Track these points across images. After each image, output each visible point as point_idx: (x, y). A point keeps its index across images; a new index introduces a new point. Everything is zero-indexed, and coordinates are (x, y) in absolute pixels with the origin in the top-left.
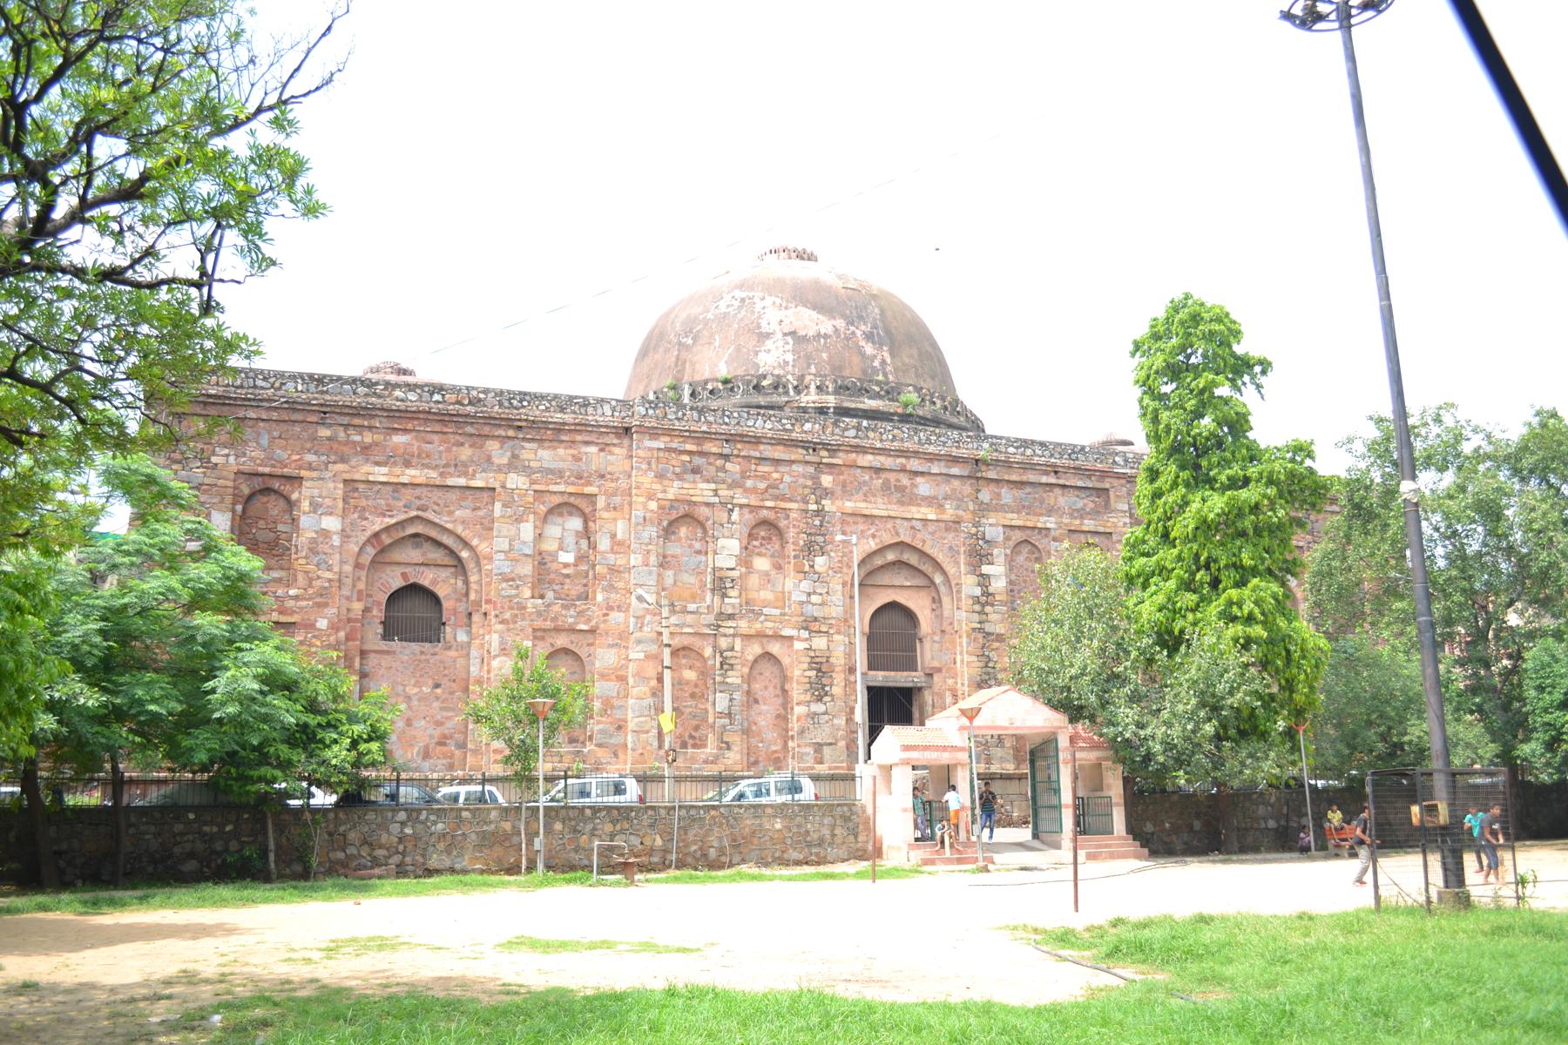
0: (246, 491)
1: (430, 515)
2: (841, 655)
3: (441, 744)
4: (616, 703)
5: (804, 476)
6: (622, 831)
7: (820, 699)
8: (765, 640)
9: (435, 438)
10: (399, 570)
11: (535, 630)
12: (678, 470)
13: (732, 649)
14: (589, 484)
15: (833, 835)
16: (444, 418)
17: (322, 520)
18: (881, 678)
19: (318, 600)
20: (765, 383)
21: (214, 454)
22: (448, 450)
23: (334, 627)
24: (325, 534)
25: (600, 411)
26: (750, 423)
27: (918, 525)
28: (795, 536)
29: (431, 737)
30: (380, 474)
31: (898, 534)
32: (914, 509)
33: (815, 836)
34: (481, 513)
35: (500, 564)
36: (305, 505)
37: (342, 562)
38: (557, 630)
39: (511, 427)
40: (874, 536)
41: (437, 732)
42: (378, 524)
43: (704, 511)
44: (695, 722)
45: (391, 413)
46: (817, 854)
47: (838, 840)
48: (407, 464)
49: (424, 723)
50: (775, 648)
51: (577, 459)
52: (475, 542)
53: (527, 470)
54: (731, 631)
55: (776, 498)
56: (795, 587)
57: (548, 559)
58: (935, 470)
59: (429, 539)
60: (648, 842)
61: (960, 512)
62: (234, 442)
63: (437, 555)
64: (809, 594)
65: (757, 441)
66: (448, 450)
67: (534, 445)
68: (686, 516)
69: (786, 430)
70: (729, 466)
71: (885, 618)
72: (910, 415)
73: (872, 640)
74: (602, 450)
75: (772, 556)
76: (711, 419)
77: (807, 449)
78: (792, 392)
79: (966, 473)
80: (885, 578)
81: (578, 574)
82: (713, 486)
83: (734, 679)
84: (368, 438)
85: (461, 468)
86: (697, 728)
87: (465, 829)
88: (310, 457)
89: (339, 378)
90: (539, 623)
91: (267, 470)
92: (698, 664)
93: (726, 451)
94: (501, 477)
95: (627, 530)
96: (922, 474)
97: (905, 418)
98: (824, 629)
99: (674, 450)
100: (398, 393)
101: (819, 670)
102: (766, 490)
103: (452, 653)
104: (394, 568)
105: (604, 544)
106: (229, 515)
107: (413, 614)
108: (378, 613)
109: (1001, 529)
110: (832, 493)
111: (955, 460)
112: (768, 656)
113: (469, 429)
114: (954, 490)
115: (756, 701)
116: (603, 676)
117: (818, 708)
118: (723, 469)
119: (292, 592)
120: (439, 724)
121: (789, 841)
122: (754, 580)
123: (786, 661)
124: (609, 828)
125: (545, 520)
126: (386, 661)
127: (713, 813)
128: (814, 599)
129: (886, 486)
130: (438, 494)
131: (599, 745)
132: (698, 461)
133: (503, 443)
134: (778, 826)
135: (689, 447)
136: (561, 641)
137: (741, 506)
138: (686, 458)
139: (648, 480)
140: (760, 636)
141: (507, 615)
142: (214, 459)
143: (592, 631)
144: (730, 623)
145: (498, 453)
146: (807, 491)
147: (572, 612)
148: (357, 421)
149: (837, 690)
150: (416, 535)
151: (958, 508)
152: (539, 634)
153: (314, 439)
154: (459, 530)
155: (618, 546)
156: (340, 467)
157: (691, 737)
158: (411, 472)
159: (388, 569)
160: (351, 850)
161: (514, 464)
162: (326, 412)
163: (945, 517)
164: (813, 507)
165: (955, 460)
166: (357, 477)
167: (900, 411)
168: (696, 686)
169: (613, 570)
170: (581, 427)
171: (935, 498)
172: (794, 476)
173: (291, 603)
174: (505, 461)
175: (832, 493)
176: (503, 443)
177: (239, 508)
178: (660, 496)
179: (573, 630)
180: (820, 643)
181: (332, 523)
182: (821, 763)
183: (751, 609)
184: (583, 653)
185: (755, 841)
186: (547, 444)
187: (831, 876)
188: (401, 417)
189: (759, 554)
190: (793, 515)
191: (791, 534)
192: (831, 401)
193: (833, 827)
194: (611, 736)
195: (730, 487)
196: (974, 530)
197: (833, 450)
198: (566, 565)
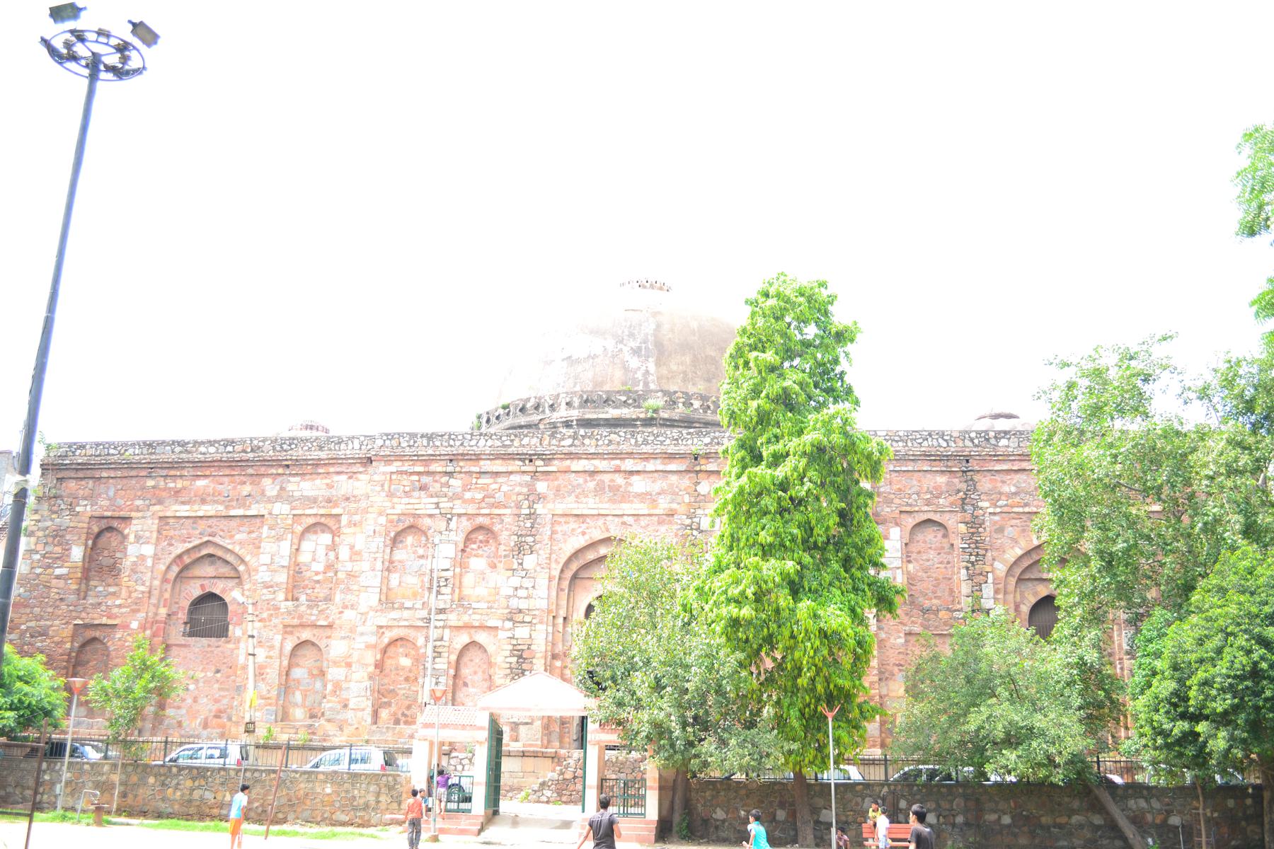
0: (96, 529)
1: (217, 540)
2: (543, 642)
3: (217, 716)
4: (344, 685)
5: (520, 485)
6: (199, 787)
8: (473, 631)
9: (226, 479)
10: (199, 582)
11: (285, 626)
12: (407, 489)
13: (441, 639)
14: (336, 506)
15: (378, 802)
16: (232, 464)
17: (142, 550)
19: (134, 607)
21: (78, 505)
22: (234, 488)
23: (143, 628)
24: (142, 558)
25: (350, 446)
26: (473, 443)
27: (630, 520)
28: (507, 539)
29: (210, 711)
30: (183, 510)
31: (608, 530)
32: (624, 506)
33: (362, 801)
34: (254, 535)
35: (263, 576)
36: (132, 538)
37: (153, 578)
38: (302, 626)
39: (281, 466)
40: (584, 533)
42: (180, 548)
43: (428, 521)
44: (408, 703)
45: (197, 464)
46: (361, 817)
47: (383, 806)
48: (203, 501)
49: (220, 702)
50: (481, 637)
51: (330, 486)
52: (247, 559)
53: (290, 499)
54: (441, 624)
55: (492, 506)
56: (503, 581)
57: (304, 568)
59: (220, 558)
60: (219, 797)
61: (674, 506)
62: (91, 497)
63: (224, 570)
64: (516, 589)
65: (477, 458)
66: (234, 488)
67: (298, 479)
68: (411, 527)
69: (504, 446)
70: (452, 482)
72: (652, 419)
74: (350, 478)
76: (438, 443)
77: (523, 460)
78: (547, 411)
79: (683, 468)
81: (326, 580)
82: (435, 500)
83: (442, 664)
84: (180, 484)
85: (242, 501)
86: (409, 707)
87: (84, 778)
88: (139, 502)
89: (164, 442)
90: (288, 621)
91: (109, 514)
92: (413, 652)
93: (450, 469)
94: (269, 506)
95: (363, 539)
96: (638, 472)
97: (648, 422)
98: (528, 619)
99: (406, 473)
100: (202, 449)
101: (520, 657)
102: (483, 500)
105: (344, 553)
106: (82, 548)
107: (208, 616)
108: (183, 616)
110: (545, 498)
111: (671, 457)
112: (473, 643)
113: (250, 471)
115: (466, 685)
116: (336, 663)
118: (447, 485)
119: (118, 602)
120: (217, 701)
121: (337, 805)
122: (468, 580)
123: (491, 649)
124: (189, 783)
125: (302, 536)
126: (183, 652)
127: (273, 776)
128: (522, 593)
130: (224, 522)
131: (329, 721)
132: (425, 479)
133: (274, 479)
134: (328, 790)
136: (306, 635)
137: (459, 515)
138: (415, 478)
139: (380, 499)
140: (467, 627)
141: (265, 615)
142: (78, 509)
143: (330, 626)
145: (270, 487)
146: (521, 497)
147: (315, 612)
148: (172, 472)
150: (211, 556)
152: (288, 629)
153: (143, 488)
154: (237, 549)
155: (355, 554)
156: (157, 508)
157: (403, 714)
159: (192, 582)
160: (10, 790)
161: (282, 496)
162: (152, 468)
163: (657, 512)
164: (527, 511)
165: (671, 457)
166: (168, 514)
167: (642, 416)
168: (410, 671)
169: (350, 575)
170: (334, 461)
171: (647, 494)
172: (514, 485)
173: (115, 610)
174: (275, 493)
175: (545, 498)
176: (274, 479)
177: (90, 542)
178: (389, 511)
179: (315, 626)
180: (522, 632)
181: (148, 550)
182: (517, 740)
183: (462, 603)
184: (322, 644)
185: (308, 802)
186: (308, 477)
187: (284, 833)
188: (203, 467)
190: (507, 520)
191: (504, 536)
192: (575, 414)
193: (378, 794)
194: (338, 713)
195: (451, 499)
196: (688, 522)
197: (547, 459)
198: (317, 573)
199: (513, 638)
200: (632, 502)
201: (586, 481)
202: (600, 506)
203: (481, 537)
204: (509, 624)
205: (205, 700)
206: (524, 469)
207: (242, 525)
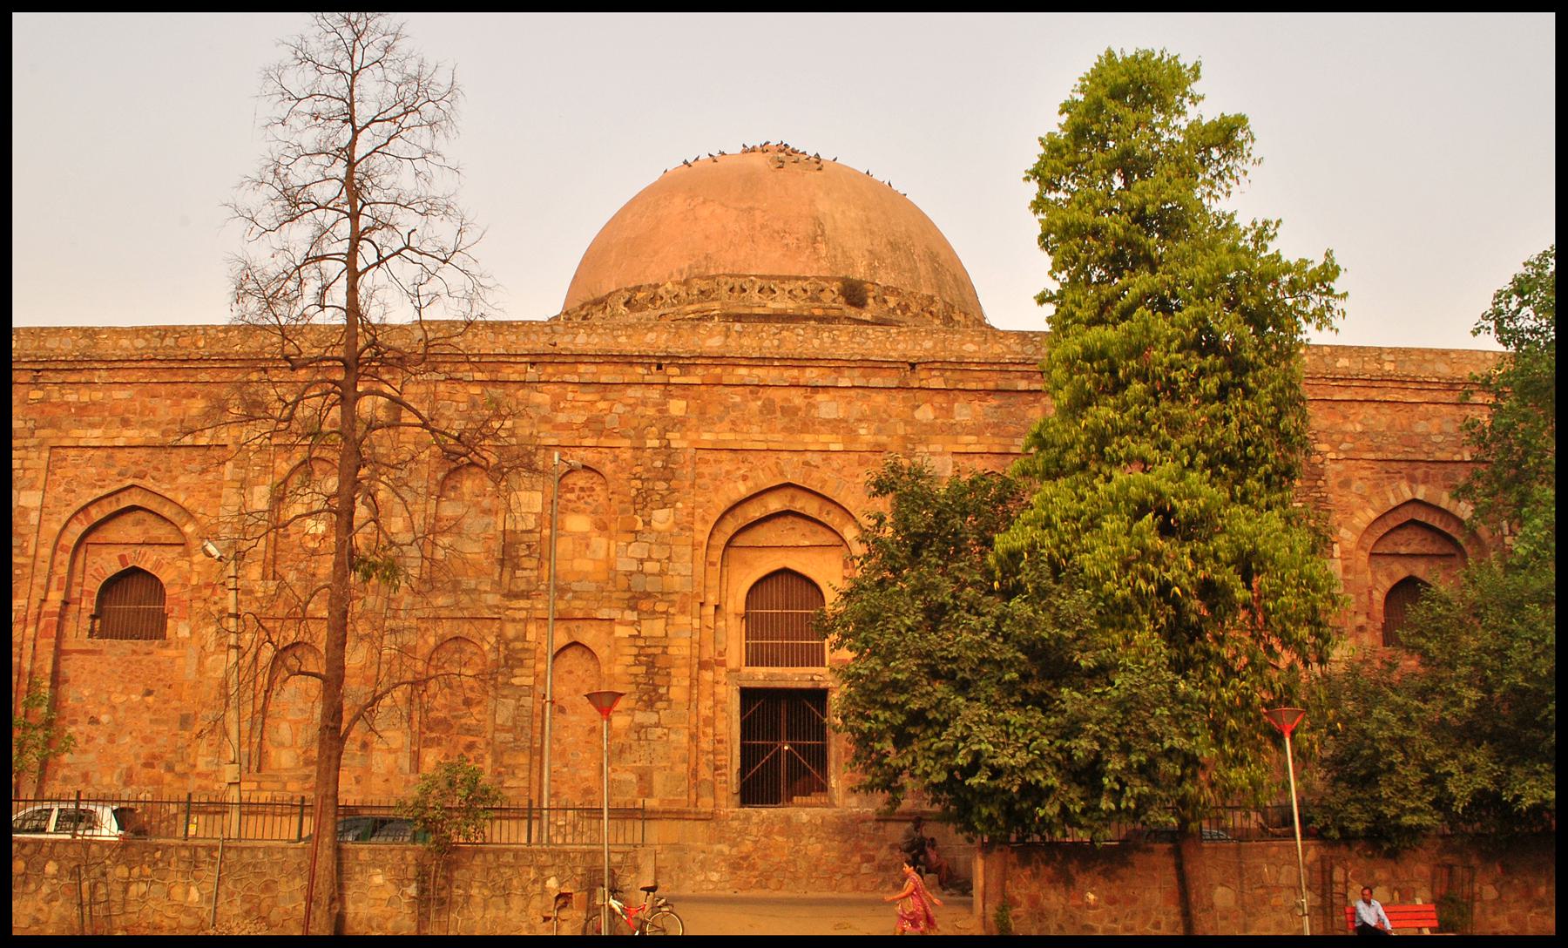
1: (148, 483)
7: (650, 705)
9: (163, 390)
18: (761, 676)
20: (639, 296)
27: (816, 459)
31: (782, 473)
32: (808, 438)
34: (210, 477)
39: (254, 368)
40: (745, 478)
41: (145, 751)
48: (126, 423)
50: (588, 636)
54: (523, 614)
65: (578, 358)
71: (776, 591)
73: (753, 622)
75: (594, 512)
80: (763, 535)
84: (85, 396)
103: (170, 652)
104: (112, 549)
109: (949, 459)
111: (877, 366)
113: (203, 377)
117: (648, 718)
120: (147, 740)
123: (603, 653)
128: (650, 567)
129: (768, 408)
135: (478, 376)
144: (523, 603)
148: (74, 378)
149: (678, 692)
151: (879, 431)
154: (181, 498)
158: (129, 433)
163: (857, 447)
180: (655, 627)
189: (574, 511)
197: (686, 363)
199: (638, 636)
200: (817, 432)
202: (769, 437)
203: (581, 483)
204: (631, 616)
205: (128, 739)
206: (648, 379)
207: (191, 460)
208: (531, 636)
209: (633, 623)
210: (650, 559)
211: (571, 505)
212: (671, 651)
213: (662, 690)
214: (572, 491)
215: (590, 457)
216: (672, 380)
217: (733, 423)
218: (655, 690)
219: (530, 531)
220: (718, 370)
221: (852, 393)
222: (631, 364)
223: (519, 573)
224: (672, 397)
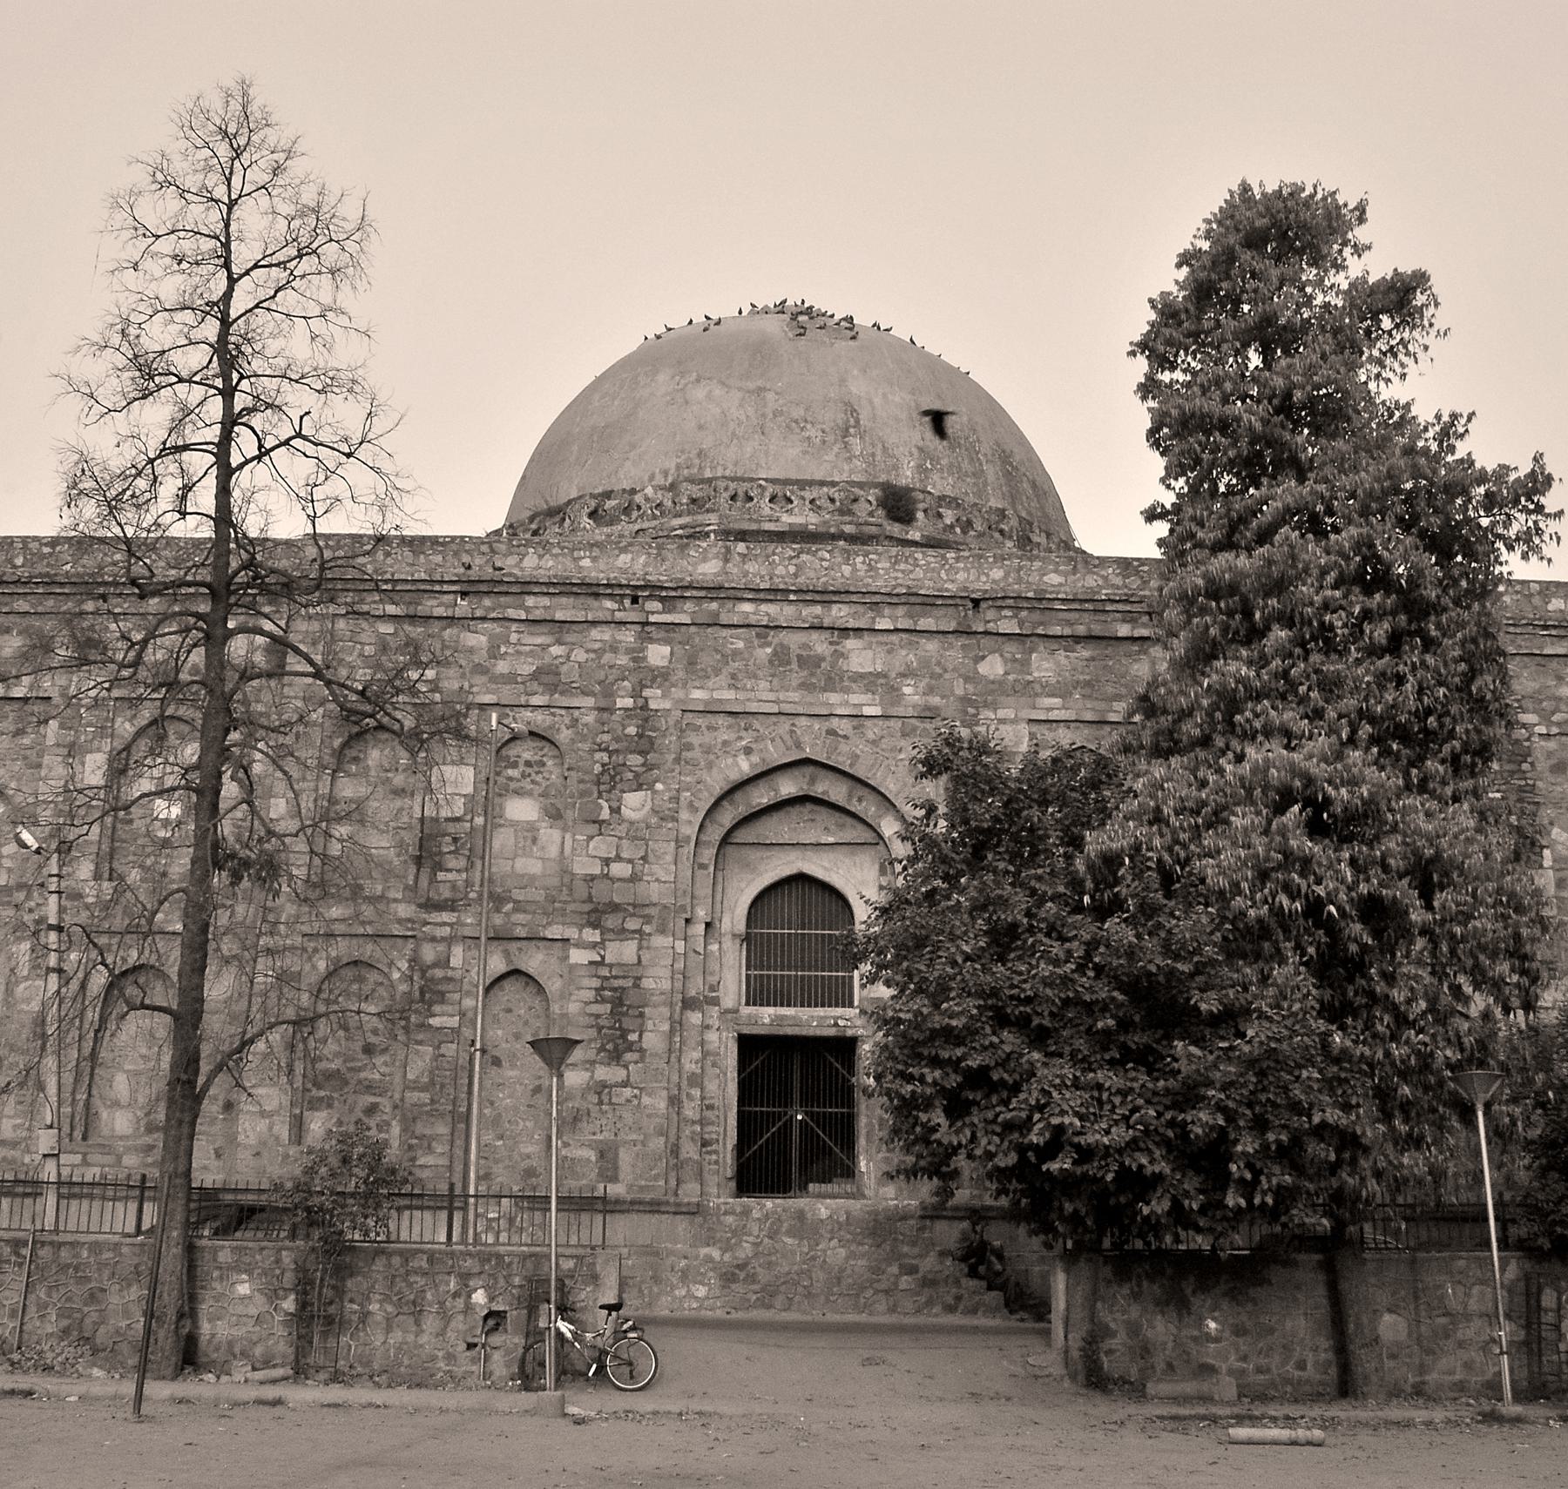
7: (615, 1057)
18: (767, 1018)
20: (610, 504)
27: (844, 726)
31: (798, 745)
32: (834, 698)
40: (748, 751)
50: (534, 961)
58: (883, 624)
61: (936, 700)
65: (526, 587)
71: (788, 904)
79: (952, 626)
80: (777, 828)
98: (632, 924)
109: (1024, 729)
111: (928, 603)
113: (22, 605)
114: (925, 663)
123: (553, 986)
128: (618, 869)
129: (781, 658)
138: (387, 628)
144: (446, 917)
149: (653, 1040)
151: (930, 690)
180: (626, 951)
182: (614, 1179)
189: (518, 793)
197: (670, 595)
199: (601, 963)
200: (847, 691)
201: (749, 646)
203: (527, 756)
204: (592, 935)
206: (619, 616)
208: (456, 961)
209: (594, 946)
210: (618, 858)
211: (513, 785)
212: (647, 983)
213: (633, 1037)
214: (515, 765)
215: (540, 719)
216: (652, 619)
217: (733, 676)
218: (623, 1036)
219: (457, 819)
220: (714, 605)
221: (894, 638)
222: (597, 595)
223: (441, 876)
224: (651, 640)
